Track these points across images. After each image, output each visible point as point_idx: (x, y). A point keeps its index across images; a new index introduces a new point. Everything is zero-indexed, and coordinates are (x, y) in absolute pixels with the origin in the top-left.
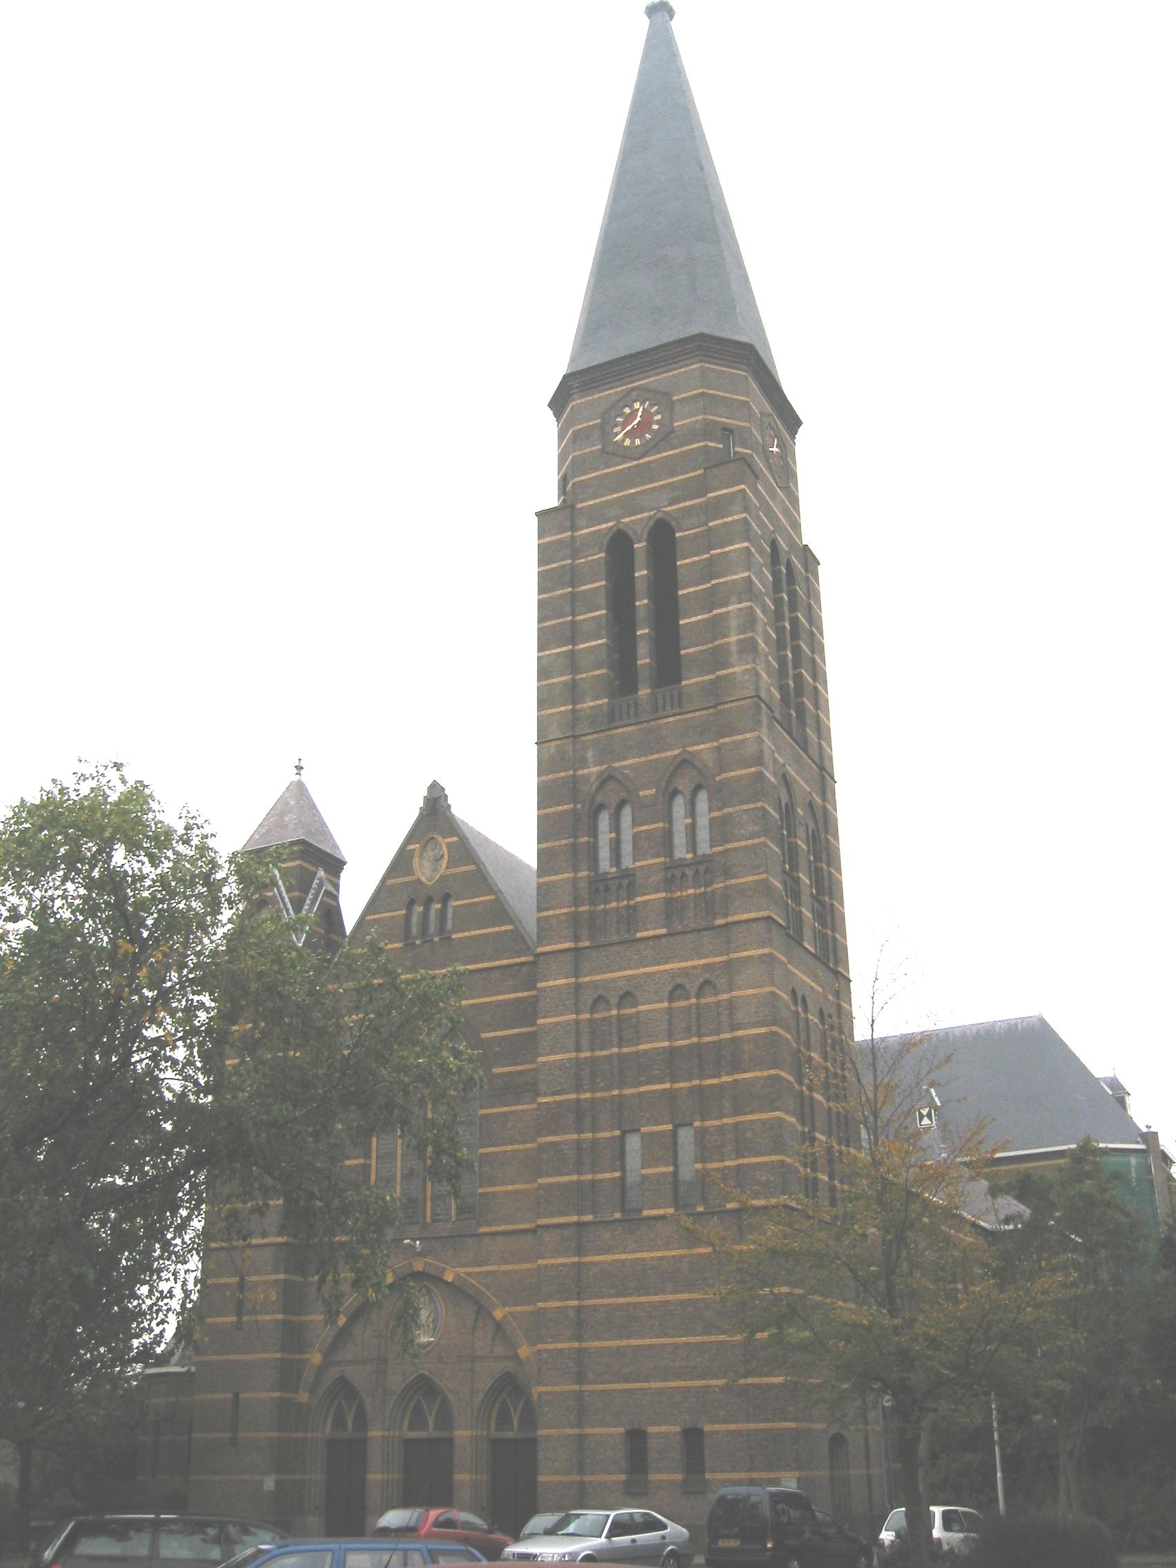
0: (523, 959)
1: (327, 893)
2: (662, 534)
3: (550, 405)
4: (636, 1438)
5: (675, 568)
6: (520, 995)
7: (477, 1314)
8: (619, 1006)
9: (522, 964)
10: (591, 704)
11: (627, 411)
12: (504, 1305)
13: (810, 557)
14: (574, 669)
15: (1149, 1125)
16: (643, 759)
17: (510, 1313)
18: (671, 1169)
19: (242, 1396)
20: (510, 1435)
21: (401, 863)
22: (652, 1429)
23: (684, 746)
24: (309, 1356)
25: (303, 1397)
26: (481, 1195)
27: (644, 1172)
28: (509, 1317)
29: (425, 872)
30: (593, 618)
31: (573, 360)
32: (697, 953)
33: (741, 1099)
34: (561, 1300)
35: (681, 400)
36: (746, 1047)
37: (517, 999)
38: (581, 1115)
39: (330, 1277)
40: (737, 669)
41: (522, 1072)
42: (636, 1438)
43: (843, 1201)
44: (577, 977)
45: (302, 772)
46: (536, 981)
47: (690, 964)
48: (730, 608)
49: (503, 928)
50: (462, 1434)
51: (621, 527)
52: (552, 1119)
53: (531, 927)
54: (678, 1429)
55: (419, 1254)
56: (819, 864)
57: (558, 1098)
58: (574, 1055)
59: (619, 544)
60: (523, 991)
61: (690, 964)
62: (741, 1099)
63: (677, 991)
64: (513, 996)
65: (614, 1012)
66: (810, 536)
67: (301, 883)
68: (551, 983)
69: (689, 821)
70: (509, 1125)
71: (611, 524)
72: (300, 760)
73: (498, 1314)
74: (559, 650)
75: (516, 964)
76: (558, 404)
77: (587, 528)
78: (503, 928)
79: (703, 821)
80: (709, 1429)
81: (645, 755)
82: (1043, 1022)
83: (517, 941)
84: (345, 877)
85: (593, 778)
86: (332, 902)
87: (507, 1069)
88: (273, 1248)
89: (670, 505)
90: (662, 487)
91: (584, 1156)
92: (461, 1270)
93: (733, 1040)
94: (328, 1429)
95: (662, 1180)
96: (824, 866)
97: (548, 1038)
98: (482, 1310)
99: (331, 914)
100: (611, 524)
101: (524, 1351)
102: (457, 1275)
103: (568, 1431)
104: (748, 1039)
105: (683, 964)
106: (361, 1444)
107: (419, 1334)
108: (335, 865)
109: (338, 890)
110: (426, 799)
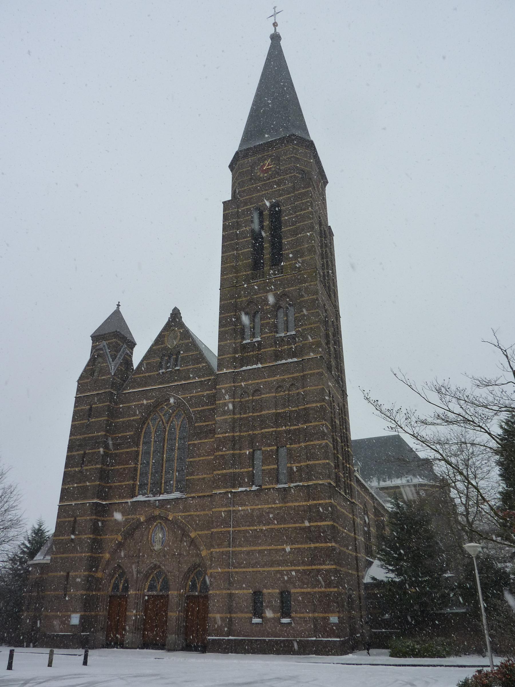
1: (127, 354)
4: (257, 594)
8: (253, 395)
11: (262, 164)
12: (195, 530)
13: (331, 233)
14: (237, 272)
18: (276, 466)
19: (70, 574)
21: (160, 339)
22: (265, 591)
24: (104, 555)
25: (99, 575)
26: (187, 480)
27: (263, 468)
28: (197, 536)
29: (171, 343)
31: (241, 145)
33: (307, 435)
36: (311, 412)
38: (234, 442)
42: (257, 594)
43: (40, 539)
44: (234, 399)
45: (120, 307)
46: (216, 385)
50: (173, 593)
52: (222, 442)
53: (214, 363)
54: (278, 591)
55: (157, 507)
58: (232, 416)
62: (307, 435)
63: (279, 387)
65: (251, 398)
66: (331, 223)
67: (116, 349)
69: (285, 318)
72: (119, 302)
73: (193, 535)
76: (231, 167)
79: (291, 318)
80: (293, 591)
83: (209, 370)
84: (135, 349)
86: (129, 358)
91: (237, 460)
93: (305, 409)
94: (110, 589)
98: (185, 534)
99: (128, 362)
101: (204, 553)
102: (175, 517)
103: (224, 592)
104: (313, 409)
106: (124, 598)
108: (132, 344)
109: (132, 355)
110: (171, 314)
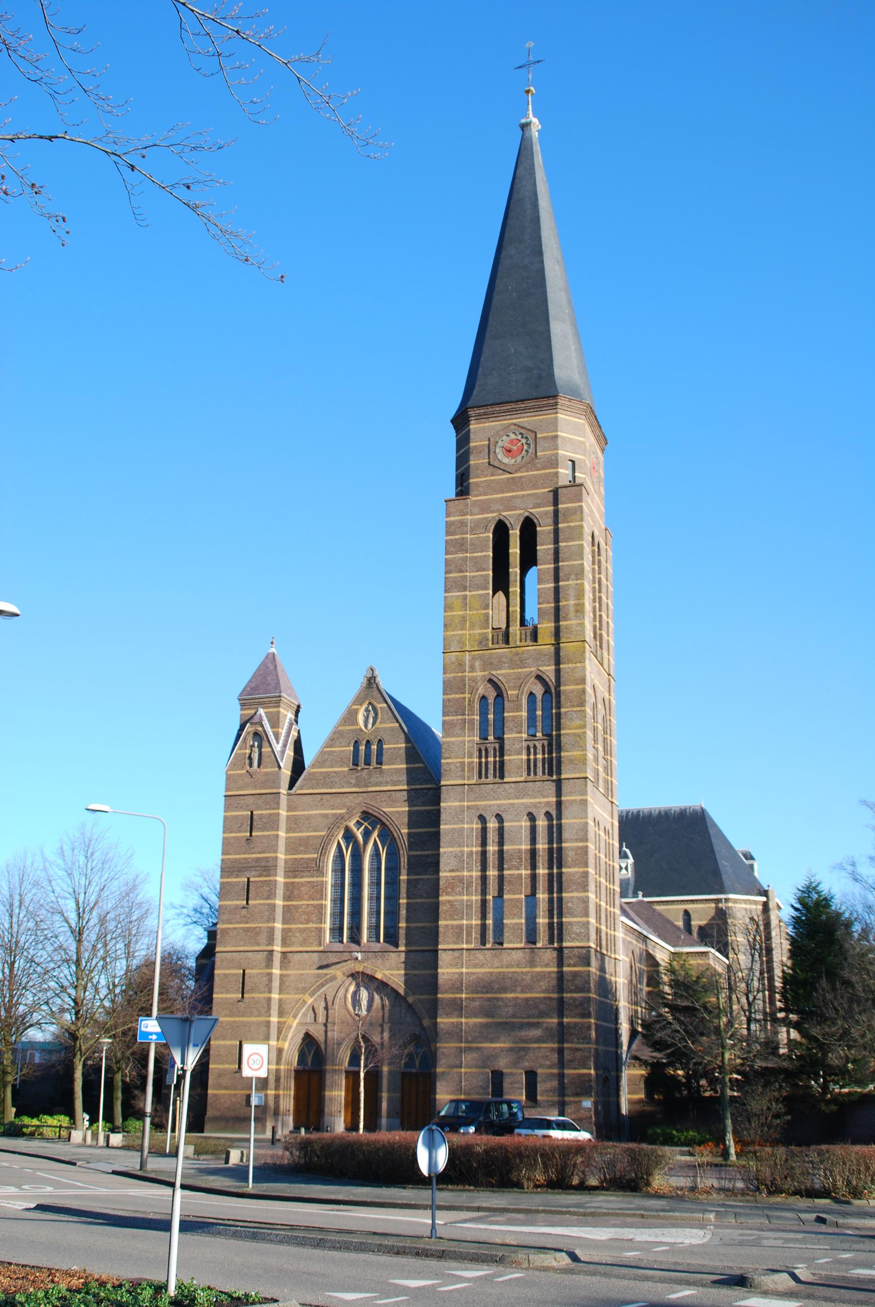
0: (429, 786)
2: (529, 527)
3: (452, 421)
5: (535, 551)
6: (427, 808)
7: (396, 998)
9: (429, 789)
10: (480, 631)
12: (414, 994)
15: (66, 220)
16: (512, 671)
17: (417, 999)
20: (414, 1071)
23: (539, 666)
30: (482, 576)
32: (542, 795)
34: (453, 993)
35: (544, 438)
37: (425, 811)
39: (7, 999)
40: (573, 622)
41: (427, 856)
47: (537, 800)
48: (571, 582)
49: (416, 765)
51: (502, 518)
56: (605, 736)
57: (453, 874)
59: (501, 531)
60: (429, 806)
61: (537, 800)
64: (423, 808)
68: (450, 804)
70: (419, 886)
71: (495, 514)
74: (459, 594)
75: (425, 789)
77: (478, 514)
78: (416, 765)
81: (513, 669)
82: (703, 811)
85: (479, 678)
87: (418, 853)
88: (266, 953)
89: (534, 508)
90: (529, 495)
92: (387, 973)
95: (516, 927)
96: (608, 737)
97: (448, 838)
100: (495, 514)
105: (533, 801)
107: (59, 1065)
